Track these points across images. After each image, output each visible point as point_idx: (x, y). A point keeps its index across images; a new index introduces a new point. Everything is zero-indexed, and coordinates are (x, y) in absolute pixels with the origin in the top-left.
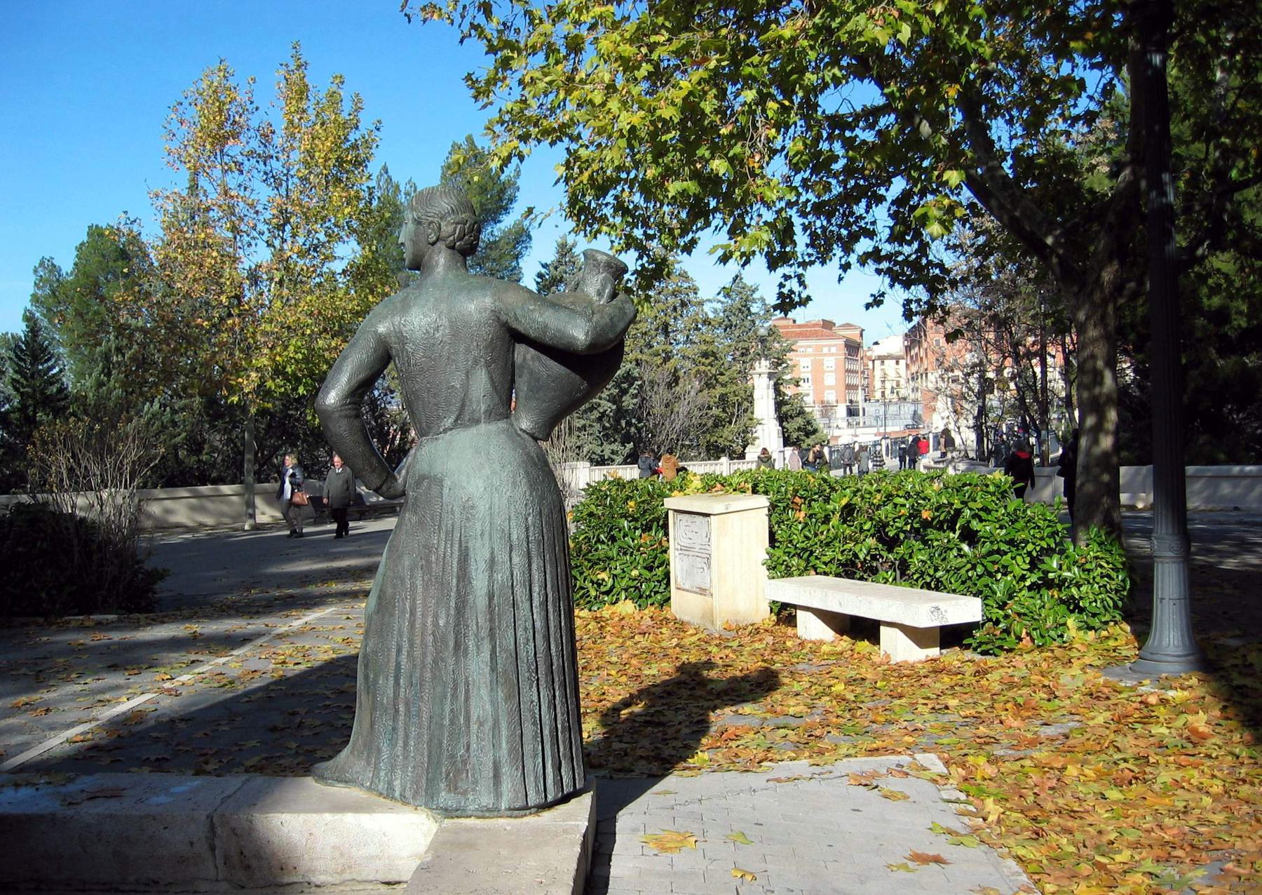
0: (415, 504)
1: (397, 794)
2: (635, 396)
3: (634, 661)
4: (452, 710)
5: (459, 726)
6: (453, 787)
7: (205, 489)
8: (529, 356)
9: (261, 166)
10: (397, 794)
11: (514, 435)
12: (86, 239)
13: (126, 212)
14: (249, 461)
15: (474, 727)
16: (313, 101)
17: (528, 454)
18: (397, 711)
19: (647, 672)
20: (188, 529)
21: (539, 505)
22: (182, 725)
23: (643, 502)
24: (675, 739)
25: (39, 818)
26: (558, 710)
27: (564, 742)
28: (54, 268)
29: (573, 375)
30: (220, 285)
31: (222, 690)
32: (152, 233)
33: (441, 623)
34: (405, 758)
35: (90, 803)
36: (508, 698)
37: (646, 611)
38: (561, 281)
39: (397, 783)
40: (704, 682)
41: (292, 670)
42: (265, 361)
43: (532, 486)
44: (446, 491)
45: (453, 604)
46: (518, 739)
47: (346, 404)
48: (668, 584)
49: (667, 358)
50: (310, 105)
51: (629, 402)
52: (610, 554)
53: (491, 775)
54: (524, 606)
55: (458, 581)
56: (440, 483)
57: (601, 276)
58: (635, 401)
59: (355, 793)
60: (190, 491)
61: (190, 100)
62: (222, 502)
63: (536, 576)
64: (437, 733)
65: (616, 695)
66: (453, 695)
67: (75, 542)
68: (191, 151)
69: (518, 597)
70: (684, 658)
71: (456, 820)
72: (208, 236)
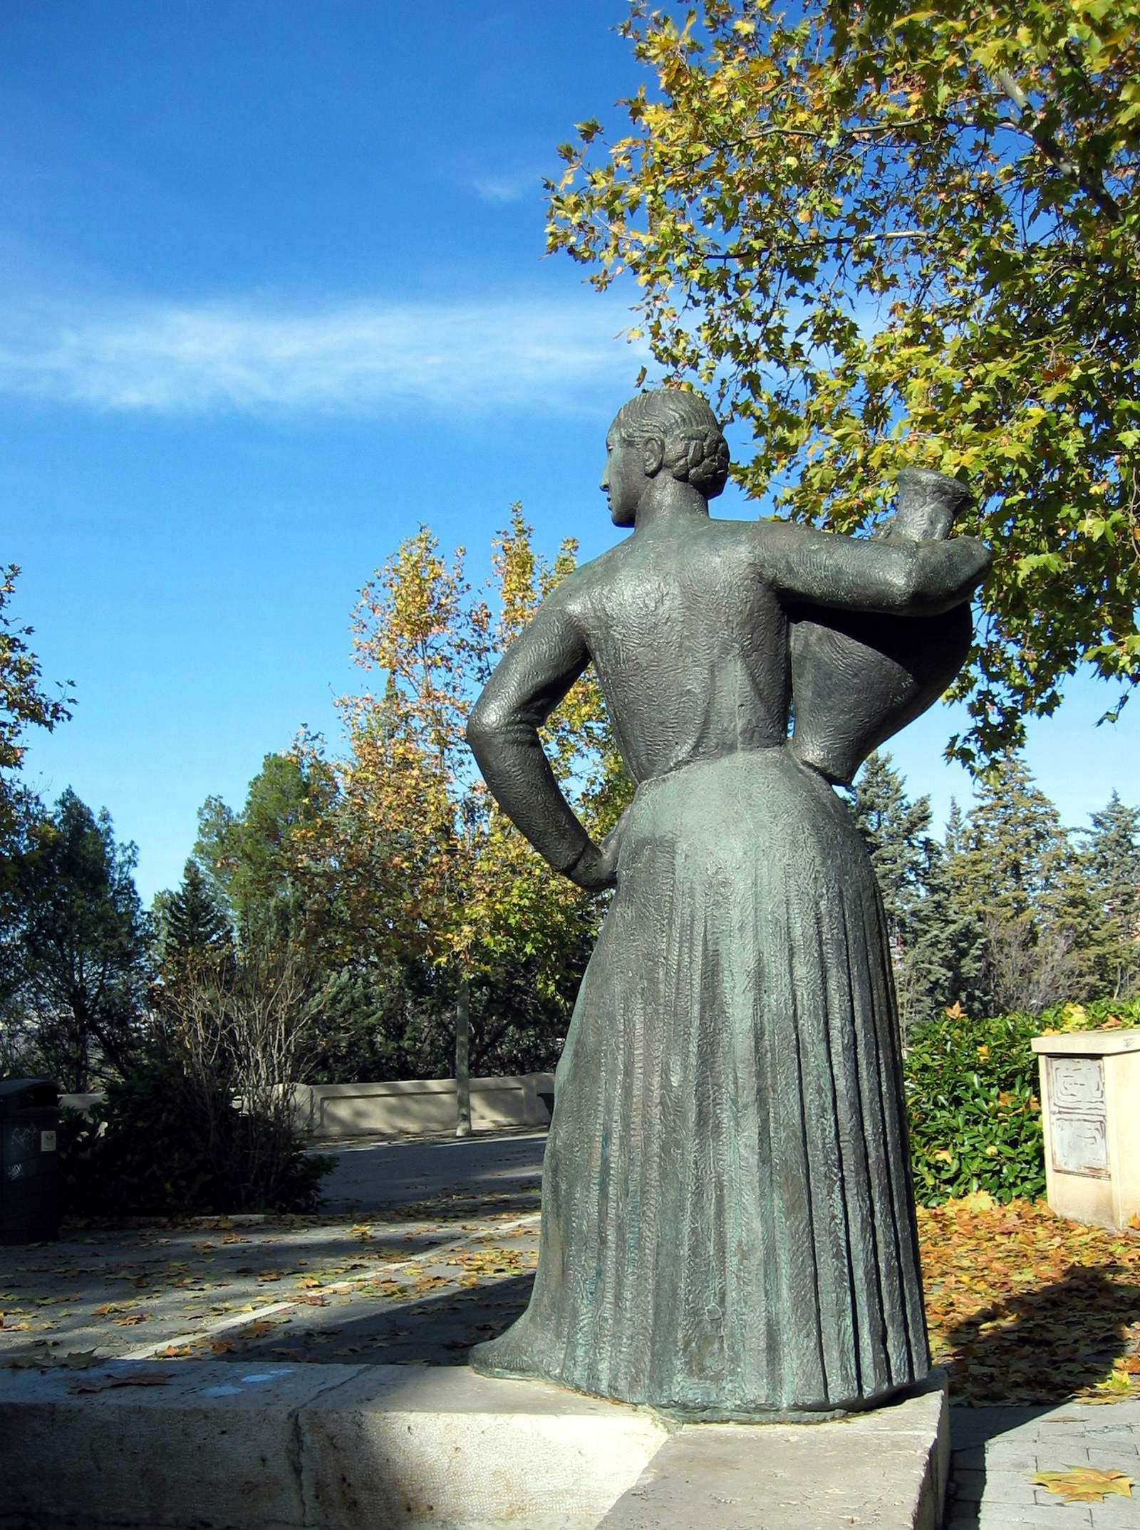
0: (631, 890)
1: (604, 1386)
2: (978, 959)
3: (996, 1265)
4: (694, 1231)
5: (707, 1257)
6: (696, 1367)
7: (406, 1085)
8: (813, 639)
9: (477, 663)
10: (604, 1386)
11: (791, 770)
12: (261, 771)
13: (305, 725)
14: (463, 1044)
15: (733, 1262)
16: (539, 574)
17: (817, 800)
18: (603, 1241)
19: (1017, 1278)
20: (383, 1136)
21: (838, 881)
22: (321, 1340)
23: (1000, 1046)
24: (1071, 1360)
25: (30, 1411)
26: (880, 1237)
27: (890, 1293)
28: (222, 810)
29: (889, 662)
30: (424, 814)
31: (388, 1299)
32: (340, 752)
33: (675, 1081)
34: (618, 1321)
35: (115, 1392)
36: (790, 1210)
37: (1010, 1207)
38: (872, 808)
39: (604, 1366)
40: (1109, 1289)
41: (490, 1277)
42: (481, 911)
43: (826, 849)
44: (679, 860)
45: (693, 1048)
46: (808, 1281)
47: (513, 723)
48: (1042, 1166)
49: (1020, 910)
50: (535, 580)
51: (970, 967)
52: (954, 1123)
53: (763, 1345)
54: (815, 1050)
55: (703, 1008)
56: (669, 847)
57: (928, 509)
58: (978, 965)
59: (538, 1387)
60: (388, 1087)
61: (383, 580)
62: (429, 1102)
63: (836, 1000)
64: (668, 1271)
65: (969, 1307)
66: (695, 1205)
67: (212, 1113)
68: (386, 643)
69: (805, 1036)
70: (1074, 1259)
71: (703, 1426)
72: (409, 750)
